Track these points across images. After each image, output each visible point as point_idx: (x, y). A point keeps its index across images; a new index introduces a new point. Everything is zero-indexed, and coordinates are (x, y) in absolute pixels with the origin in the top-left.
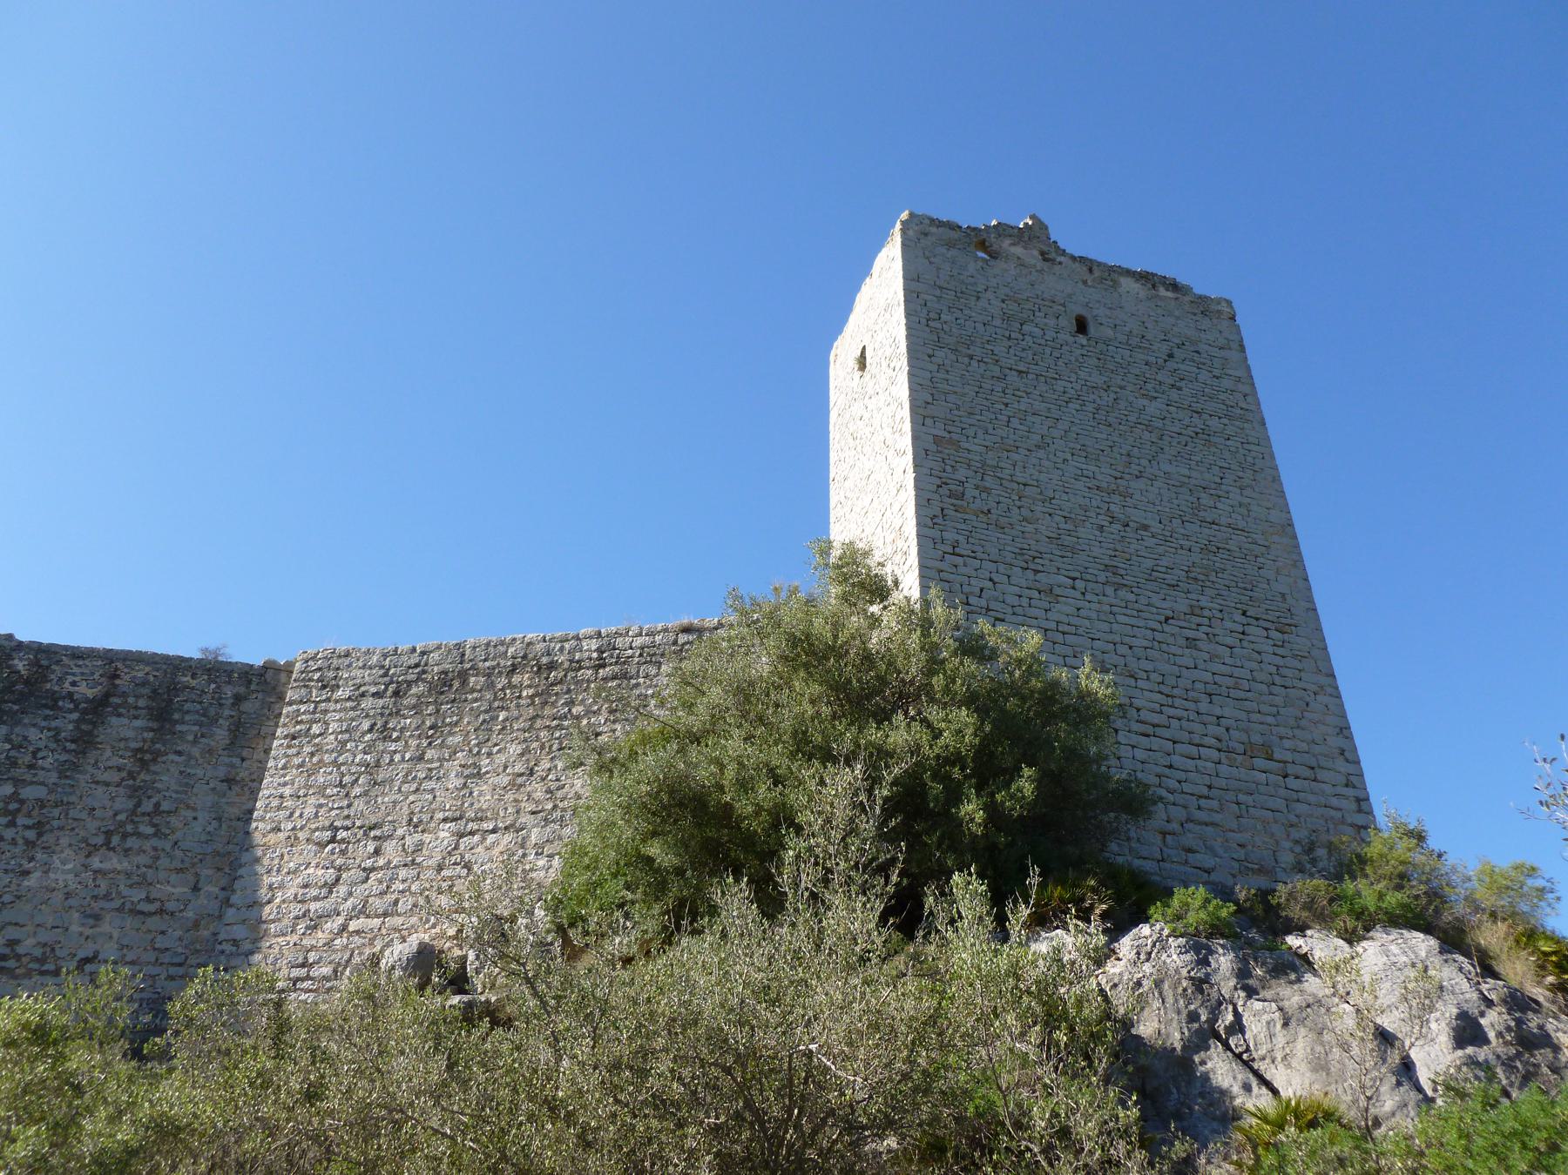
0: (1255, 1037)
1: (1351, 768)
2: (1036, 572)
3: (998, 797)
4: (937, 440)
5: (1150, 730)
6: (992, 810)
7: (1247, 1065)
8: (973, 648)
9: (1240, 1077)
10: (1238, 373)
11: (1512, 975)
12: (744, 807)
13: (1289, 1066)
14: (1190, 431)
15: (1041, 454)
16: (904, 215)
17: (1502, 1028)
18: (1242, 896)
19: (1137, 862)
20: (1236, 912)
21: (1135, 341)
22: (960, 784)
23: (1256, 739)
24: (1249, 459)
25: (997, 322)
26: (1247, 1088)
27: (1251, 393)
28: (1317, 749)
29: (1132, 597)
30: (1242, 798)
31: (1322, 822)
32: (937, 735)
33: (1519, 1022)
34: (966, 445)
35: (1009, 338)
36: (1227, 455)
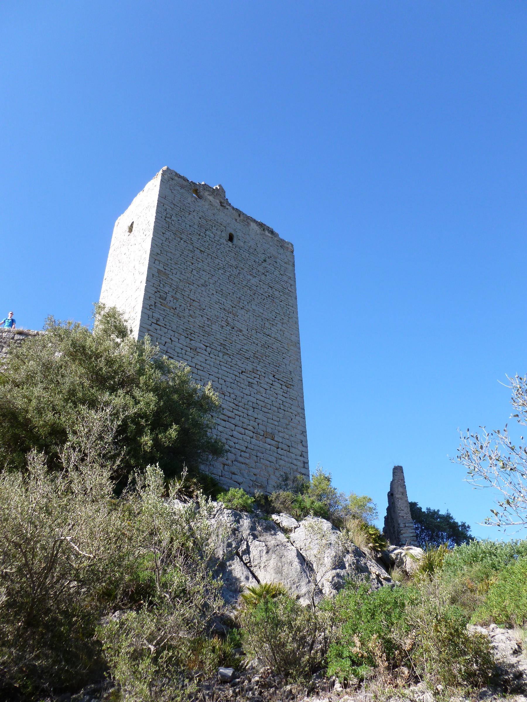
0: (254, 556)
1: (304, 449)
2: (191, 340)
3: (160, 436)
4: (159, 271)
5: (226, 419)
6: (156, 440)
7: (248, 568)
8: (160, 366)
9: (245, 573)
10: (290, 275)
11: (356, 541)
12: (38, 422)
13: (266, 570)
14: (266, 295)
15: (203, 289)
16: (165, 168)
17: (351, 563)
18: (257, 495)
19: (213, 476)
20: (254, 501)
21: (251, 251)
22: (144, 427)
23: (269, 430)
24: (288, 312)
25: (196, 227)
26: (247, 578)
27: (293, 285)
28: (292, 439)
29: (230, 360)
30: (259, 454)
31: (289, 469)
32: (137, 402)
33: (358, 561)
34: (171, 277)
35: (200, 235)
36: (279, 308)
